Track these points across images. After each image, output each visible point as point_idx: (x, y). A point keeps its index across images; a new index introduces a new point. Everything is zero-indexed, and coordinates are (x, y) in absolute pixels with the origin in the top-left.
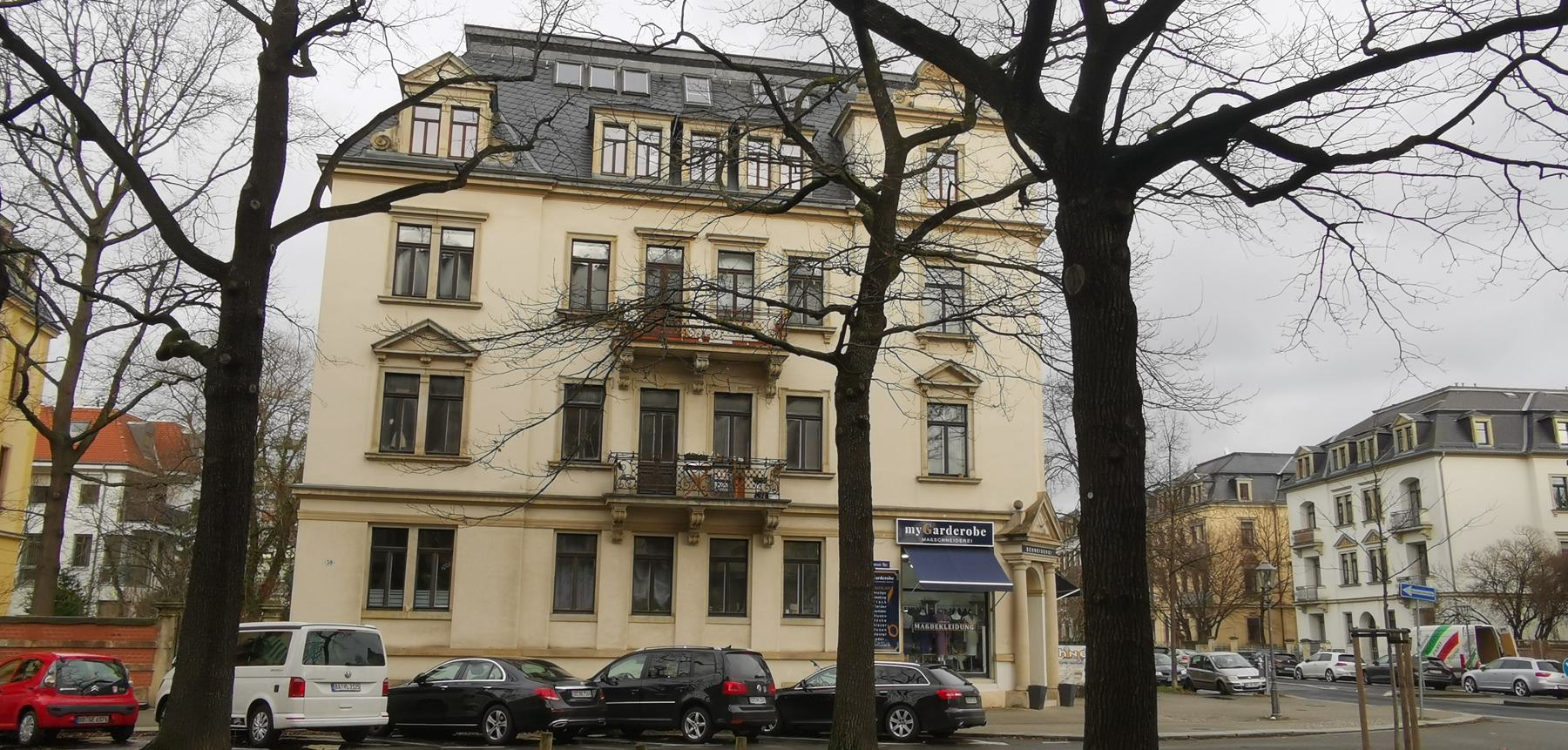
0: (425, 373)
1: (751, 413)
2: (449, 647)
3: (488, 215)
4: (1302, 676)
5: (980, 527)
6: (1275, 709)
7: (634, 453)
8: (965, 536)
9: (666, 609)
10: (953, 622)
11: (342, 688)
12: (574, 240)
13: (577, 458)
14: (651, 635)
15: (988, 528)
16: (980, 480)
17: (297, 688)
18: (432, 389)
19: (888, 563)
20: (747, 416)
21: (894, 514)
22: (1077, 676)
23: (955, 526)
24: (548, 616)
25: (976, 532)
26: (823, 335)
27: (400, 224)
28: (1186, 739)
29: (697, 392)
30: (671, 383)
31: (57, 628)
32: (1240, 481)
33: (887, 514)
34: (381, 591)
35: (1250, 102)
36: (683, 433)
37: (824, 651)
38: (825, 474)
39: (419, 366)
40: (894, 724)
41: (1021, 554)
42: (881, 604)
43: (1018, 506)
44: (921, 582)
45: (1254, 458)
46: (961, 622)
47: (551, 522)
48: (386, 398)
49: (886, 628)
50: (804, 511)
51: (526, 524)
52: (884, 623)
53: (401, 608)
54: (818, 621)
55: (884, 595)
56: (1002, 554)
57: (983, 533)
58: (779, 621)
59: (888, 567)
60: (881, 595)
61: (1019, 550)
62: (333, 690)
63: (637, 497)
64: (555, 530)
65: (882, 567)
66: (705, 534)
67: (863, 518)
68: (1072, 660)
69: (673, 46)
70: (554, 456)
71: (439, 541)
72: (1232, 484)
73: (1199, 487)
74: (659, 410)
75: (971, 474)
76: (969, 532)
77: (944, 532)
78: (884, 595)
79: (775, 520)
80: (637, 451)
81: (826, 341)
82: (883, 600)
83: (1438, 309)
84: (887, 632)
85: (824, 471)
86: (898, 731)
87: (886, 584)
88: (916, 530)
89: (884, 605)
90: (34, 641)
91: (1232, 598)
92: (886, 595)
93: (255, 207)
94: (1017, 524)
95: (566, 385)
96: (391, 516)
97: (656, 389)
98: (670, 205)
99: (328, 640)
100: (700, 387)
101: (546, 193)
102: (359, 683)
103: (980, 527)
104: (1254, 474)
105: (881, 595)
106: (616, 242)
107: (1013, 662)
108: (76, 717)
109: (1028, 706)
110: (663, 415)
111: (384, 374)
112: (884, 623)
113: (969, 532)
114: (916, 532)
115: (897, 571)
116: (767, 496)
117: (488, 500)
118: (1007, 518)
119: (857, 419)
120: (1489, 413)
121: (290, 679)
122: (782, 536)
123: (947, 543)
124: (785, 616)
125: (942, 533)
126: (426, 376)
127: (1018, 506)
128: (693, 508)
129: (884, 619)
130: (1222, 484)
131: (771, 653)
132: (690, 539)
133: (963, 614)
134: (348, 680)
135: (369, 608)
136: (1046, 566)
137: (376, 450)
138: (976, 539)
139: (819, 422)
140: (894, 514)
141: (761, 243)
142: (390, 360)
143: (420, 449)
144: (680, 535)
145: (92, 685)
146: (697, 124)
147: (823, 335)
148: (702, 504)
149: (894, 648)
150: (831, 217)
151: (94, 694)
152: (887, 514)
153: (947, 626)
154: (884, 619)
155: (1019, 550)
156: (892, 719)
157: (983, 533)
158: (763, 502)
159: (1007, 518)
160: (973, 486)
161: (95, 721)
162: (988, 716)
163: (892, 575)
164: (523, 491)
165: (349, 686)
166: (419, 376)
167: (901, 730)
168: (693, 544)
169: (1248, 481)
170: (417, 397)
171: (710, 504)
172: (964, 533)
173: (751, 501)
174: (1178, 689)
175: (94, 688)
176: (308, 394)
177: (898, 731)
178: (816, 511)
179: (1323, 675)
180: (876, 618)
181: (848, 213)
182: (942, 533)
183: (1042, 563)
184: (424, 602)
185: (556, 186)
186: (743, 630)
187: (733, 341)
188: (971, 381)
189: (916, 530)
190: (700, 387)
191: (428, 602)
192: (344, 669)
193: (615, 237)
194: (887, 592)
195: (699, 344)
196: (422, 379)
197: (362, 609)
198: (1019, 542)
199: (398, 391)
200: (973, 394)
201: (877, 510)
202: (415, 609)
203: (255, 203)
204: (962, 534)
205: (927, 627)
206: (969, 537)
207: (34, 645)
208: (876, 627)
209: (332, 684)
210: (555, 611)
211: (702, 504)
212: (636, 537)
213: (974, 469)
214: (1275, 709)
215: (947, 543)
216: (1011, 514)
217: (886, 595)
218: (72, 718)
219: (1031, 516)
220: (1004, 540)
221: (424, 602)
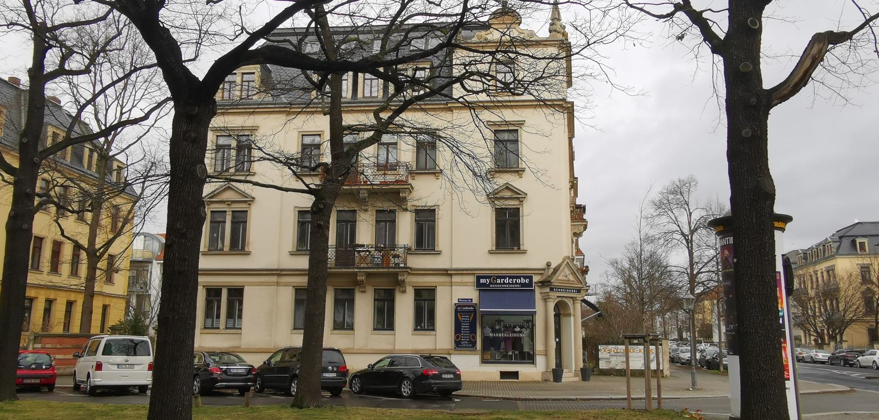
0: (229, 210)
1: (395, 220)
2: (240, 347)
3: (258, 127)
4: (877, 366)
5: (525, 278)
6: (694, 384)
7: (372, 245)
8: (516, 283)
9: (351, 327)
10: (515, 332)
11: (124, 366)
12: (303, 135)
13: (305, 249)
14: (382, 342)
15: (531, 278)
16: (527, 250)
17: (99, 367)
18: (233, 217)
19: (472, 299)
20: (393, 222)
21: (474, 272)
22: (623, 363)
23: (510, 277)
24: (290, 331)
25: (523, 281)
26: (435, 174)
27: (217, 136)
28: (575, 400)
29: (366, 210)
30: (353, 206)
31: (70, 339)
32: (858, 240)
33: (470, 272)
34: (211, 320)
35: (249, 36)
36: (358, 232)
37: (436, 349)
38: (521, 251)
39: (226, 206)
40: (404, 388)
41: (549, 292)
42: (466, 323)
43: (549, 265)
45: (872, 225)
46: (520, 332)
47: (291, 282)
48: (212, 224)
49: (470, 336)
50: (423, 272)
51: (278, 284)
52: (468, 333)
53: (218, 328)
54: (433, 333)
56: (540, 293)
57: (527, 281)
58: (411, 333)
59: (472, 302)
60: (466, 318)
61: (548, 290)
62: (118, 368)
63: (334, 268)
64: (293, 286)
65: (468, 302)
66: (331, 287)
67: (316, 277)
68: (619, 354)
69: (610, 6)
70: (293, 249)
71: (237, 293)
72: (854, 243)
73: (830, 245)
74: (347, 222)
75: (246, 249)
76: (518, 281)
77: (504, 281)
79: (402, 278)
80: (374, 244)
81: (520, 176)
82: (468, 320)
84: (470, 338)
85: (436, 250)
86: (405, 392)
87: (469, 312)
88: (486, 281)
89: (468, 323)
90: (61, 345)
91: (851, 316)
92: (469, 318)
93: (25, 142)
94: (547, 276)
95: (299, 211)
96: (226, 282)
97: (344, 211)
98: (459, 108)
99: (136, 344)
100: (365, 208)
101: (287, 112)
102: (134, 364)
103: (525, 278)
104: (870, 236)
105: (466, 318)
106: (323, 134)
107: (546, 355)
108: (23, 380)
109: (552, 380)
111: (209, 212)
112: (468, 333)
113: (518, 281)
115: (476, 304)
116: (399, 265)
117: (258, 272)
118: (542, 272)
119: (317, 224)
121: (96, 362)
122: (413, 286)
123: (505, 287)
124: (415, 330)
125: (502, 282)
126: (230, 211)
127: (549, 265)
128: (358, 273)
129: (468, 331)
130: (846, 242)
131: (346, 349)
132: (361, 290)
133: (521, 327)
134: (126, 363)
135: (205, 328)
136: (574, 299)
137: (494, 248)
138: (523, 285)
140: (474, 272)
141: (521, 124)
142: (213, 205)
143: (227, 248)
144: (357, 287)
145: (31, 365)
147: (435, 174)
148: (361, 270)
149: (474, 347)
150: (514, 105)
151: (33, 369)
152: (470, 272)
153: (509, 335)
154: (468, 331)
155: (548, 290)
156: (403, 386)
157: (527, 281)
158: (397, 268)
159: (542, 272)
160: (247, 256)
161: (33, 382)
162: (463, 385)
163: (473, 306)
164: (276, 267)
165: (127, 366)
166: (226, 211)
167: (406, 392)
168: (364, 292)
169: (865, 240)
170: (225, 222)
171: (368, 270)
172: (516, 281)
173: (392, 268)
174: (723, 372)
175: (33, 366)
177: (405, 392)
178: (430, 272)
179: (871, 364)
180: (463, 328)
181: (447, 105)
182: (502, 282)
183: (572, 297)
184: (230, 325)
185: (291, 108)
186: (391, 338)
187: (380, 182)
188: (521, 195)
189: (486, 281)
190: (365, 208)
191: (232, 325)
192: (125, 357)
193: (323, 131)
194: (470, 316)
195: (362, 185)
196: (227, 213)
197: (201, 329)
198: (548, 286)
199: (218, 220)
200: (250, 204)
201: (201, 270)
202: (226, 328)
203: (25, 140)
204: (514, 282)
205: (505, 335)
206: (518, 284)
207: (61, 347)
209: (118, 365)
210: (374, 329)
211: (361, 270)
212: (375, 289)
213: (523, 245)
214: (694, 384)
215: (505, 287)
216: (544, 270)
217: (469, 318)
218: (21, 380)
219: (556, 270)
220: (540, 284)
221: (230, 325)
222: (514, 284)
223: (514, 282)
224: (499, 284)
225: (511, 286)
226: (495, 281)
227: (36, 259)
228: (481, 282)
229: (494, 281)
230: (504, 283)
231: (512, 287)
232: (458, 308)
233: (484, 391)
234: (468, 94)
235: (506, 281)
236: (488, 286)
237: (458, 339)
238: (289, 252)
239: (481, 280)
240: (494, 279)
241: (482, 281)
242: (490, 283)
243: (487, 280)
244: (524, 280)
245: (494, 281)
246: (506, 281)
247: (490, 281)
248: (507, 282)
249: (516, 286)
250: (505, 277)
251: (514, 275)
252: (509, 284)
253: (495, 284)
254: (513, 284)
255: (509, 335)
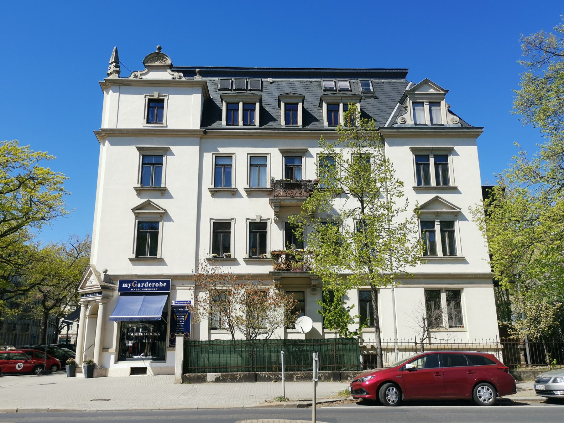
5: (163, 282)
8: (155, 287)
23: (149, 282)
25: (161, 284)
44: (110, 317)
55: (183, 318)
60: (181, 318)
76: (157, 285)
78: (183, 318)
82: (182, 320)
83: (475, 204)
89: (182, 322)
105: (181, 318)
110: (314, 151)
113: (157, 285)
114: (128, 286)
120: (207, 72)
125: (142, 286)
138: (160, 288)
139: (228, 108)
146: (376, 339)
153: (145, 334)
172: (155, 285)
176: (403, 194)
180: (178, 327)
182: (142, 286)
194: (185, 316)
204: (153, 286)
208: (178, 329)
222: (153, 288)
223: (153, 286)
224: (139, 288)
225: (150, 289)
226: (136, 285)
227: (297, 135)
228: (123, 286)
229: (134, 285)
230: (144, 287)
231: (151, 291)
232: (174, 309)
233: (221, 359)
234: (493, 353)
235: (146, 285)
236: (129, 290)
237: (173, 337)
238: (244, 259)
239: (123, 284)
240: (135, 283)
241: (124, 285)
242: (132, 287)
243: (129, 284)
244: (162, 284)
245: (134, 285)
246: (146, 285)
247: (131, 285)
248: (147, 286)
249: (154, 289)
250: (145, 282)
251: (154, 280)
252: (148, 287)
253: (135, 288)
254: (151, 287)
255: (145, 334)
